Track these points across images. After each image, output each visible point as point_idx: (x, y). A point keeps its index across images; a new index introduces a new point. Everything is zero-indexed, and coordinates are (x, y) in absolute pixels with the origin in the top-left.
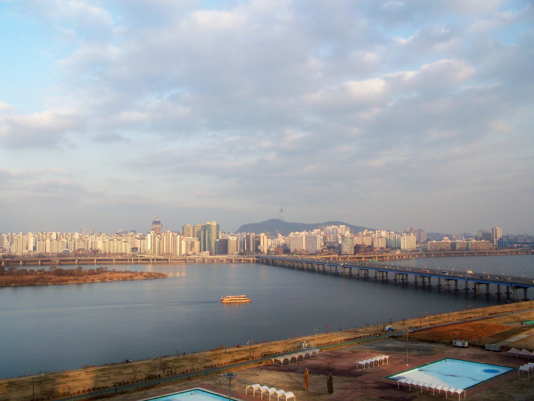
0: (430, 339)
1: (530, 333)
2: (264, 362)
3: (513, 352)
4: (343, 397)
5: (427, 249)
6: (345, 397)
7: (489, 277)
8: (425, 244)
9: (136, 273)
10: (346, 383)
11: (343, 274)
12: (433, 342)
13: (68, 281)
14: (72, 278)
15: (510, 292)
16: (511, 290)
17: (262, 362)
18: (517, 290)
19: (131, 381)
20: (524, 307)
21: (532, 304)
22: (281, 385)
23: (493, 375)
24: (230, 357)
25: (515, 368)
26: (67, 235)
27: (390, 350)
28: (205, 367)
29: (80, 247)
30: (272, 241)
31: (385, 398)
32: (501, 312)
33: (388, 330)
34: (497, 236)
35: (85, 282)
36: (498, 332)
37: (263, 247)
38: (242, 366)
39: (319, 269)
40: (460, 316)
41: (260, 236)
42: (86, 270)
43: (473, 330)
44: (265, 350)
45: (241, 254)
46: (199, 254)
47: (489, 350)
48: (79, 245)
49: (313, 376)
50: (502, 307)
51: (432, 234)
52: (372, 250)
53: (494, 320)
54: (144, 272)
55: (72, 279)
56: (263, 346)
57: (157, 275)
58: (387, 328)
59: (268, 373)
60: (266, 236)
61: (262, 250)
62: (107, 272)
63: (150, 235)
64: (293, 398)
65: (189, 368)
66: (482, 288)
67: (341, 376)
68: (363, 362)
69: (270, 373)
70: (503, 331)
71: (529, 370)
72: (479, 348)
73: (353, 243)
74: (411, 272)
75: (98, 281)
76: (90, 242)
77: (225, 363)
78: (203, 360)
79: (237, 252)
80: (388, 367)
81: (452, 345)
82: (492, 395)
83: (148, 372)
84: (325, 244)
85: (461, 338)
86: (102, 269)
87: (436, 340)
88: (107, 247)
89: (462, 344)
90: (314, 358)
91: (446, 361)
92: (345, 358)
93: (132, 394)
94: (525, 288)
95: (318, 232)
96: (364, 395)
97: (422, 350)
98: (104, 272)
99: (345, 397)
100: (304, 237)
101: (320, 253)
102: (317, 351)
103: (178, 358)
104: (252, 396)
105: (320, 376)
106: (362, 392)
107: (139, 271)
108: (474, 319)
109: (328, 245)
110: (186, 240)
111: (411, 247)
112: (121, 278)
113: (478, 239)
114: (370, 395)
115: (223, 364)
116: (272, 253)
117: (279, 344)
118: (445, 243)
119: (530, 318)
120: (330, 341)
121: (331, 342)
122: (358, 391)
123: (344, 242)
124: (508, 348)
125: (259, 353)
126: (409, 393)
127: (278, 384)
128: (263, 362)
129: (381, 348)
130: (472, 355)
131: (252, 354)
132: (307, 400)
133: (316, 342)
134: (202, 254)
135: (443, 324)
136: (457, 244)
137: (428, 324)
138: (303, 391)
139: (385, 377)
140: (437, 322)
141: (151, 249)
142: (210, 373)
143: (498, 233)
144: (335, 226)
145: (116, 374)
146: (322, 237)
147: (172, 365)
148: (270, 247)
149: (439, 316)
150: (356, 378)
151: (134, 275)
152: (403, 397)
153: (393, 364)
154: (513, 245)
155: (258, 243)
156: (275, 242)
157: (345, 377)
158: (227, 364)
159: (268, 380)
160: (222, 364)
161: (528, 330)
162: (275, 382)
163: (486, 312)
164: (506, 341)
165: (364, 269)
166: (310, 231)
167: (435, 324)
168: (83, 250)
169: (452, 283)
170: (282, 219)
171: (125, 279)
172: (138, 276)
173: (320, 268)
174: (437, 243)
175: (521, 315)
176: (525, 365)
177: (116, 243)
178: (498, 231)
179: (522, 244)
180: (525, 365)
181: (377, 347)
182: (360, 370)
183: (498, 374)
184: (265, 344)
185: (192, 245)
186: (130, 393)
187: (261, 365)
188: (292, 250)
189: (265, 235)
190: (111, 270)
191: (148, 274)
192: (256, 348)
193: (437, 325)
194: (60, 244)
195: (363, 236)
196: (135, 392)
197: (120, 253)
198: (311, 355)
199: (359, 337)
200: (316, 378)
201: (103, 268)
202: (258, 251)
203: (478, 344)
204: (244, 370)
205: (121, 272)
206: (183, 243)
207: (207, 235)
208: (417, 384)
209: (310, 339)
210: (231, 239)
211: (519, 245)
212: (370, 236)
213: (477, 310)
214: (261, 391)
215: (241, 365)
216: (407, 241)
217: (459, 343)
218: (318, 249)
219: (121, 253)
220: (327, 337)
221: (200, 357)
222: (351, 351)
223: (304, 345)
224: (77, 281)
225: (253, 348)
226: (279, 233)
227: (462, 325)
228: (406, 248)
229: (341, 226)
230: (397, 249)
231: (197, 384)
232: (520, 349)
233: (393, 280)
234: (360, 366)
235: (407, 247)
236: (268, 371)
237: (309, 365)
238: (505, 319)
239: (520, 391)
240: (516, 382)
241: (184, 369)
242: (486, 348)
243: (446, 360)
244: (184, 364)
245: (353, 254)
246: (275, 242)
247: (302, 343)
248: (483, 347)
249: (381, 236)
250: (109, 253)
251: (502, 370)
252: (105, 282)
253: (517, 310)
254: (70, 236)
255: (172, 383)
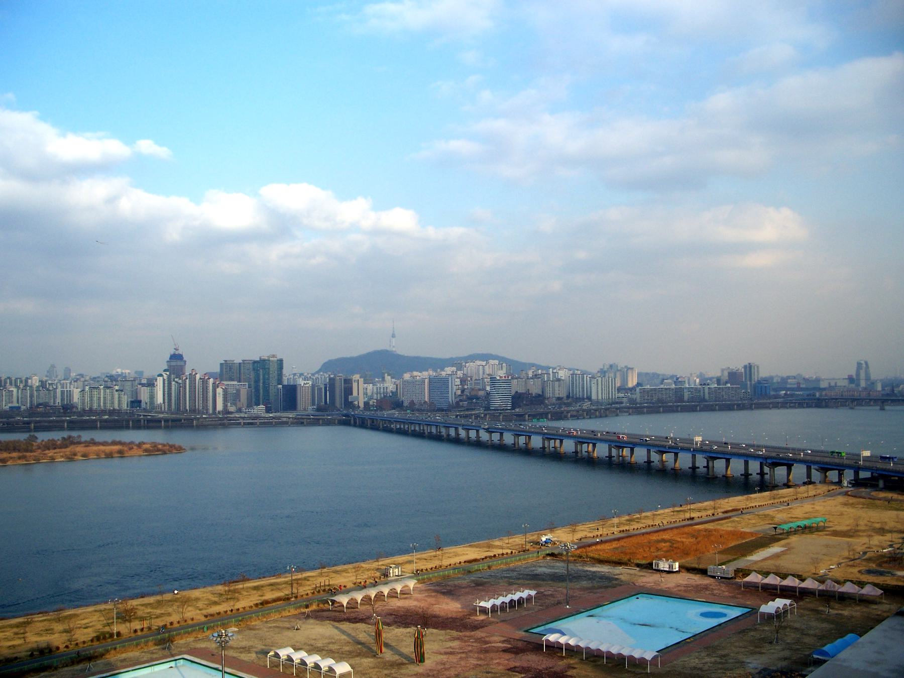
0: (614, 558)
1: (788, 544)
2: (314, 604)
3: (810, 587)
4: (444, 668)
5: (636, 400)
6: (446, 669)
7: (730, 447)
8: (633, 391)
9: (130, 445)
10: (452, 641)
11: (515, 447)
12: (619, 563)
13: (7, 461)
14: (15, 455)
15: (765, 472)
16: (766, 469)
17: (311, 604)
18: (775, 469)
19: (64, 646)
20: (784, 497)
21: (797, 493)
22: (336, 647)
23: (713, 622)
24: (257, 595)
25: (753, 609)
26: (19, 380)
27: (543, 580)
28: (206, 616)
29: (41, 401)
30: (375, 387)
31: (517, 669)
32: (744, 507)
33: (546, 542)
34: (753, 378)
35: (37, 460)
36: (733, 544)
37: (357, 398)
38: (272, 612)
39: (448, 435)
40: (673, 515)
41: (352, 379)
42: (43, 441)
43: (692, 540)
44: (322, 581)
45: (319, 409)
46: (247, 411)
47: (714, 577)
48: (38, 396)
49: (397, 630)
50: (747, 500)
51: (647, 374)
52: (542, 402)
53: (730, 522)
54: (144, 443)
55: (14, 458)
56: (321, 575)
57: (168, 448)
58: (544, 539)
59: (317, 624)
60: (363, 379)
61: (356, 403)
62: (79, 443)
63: (161, 378)
64: (349, 673)
65: (175, 618)
66: (719, 466)
67: (445, 630)
68: (487, 604)
69: (322, 625)
70: (744, 541)
71: (776, 612)
72: (698, 574)
73: (510, 391)
74: (601, 440)
75: (62, 459)
76: (59, 391)
77: (244, 608)
78: (206, 603)
79: (313, 407)
80: (533, 611)
81: (652, 569)
82: (707, 659)
83: (101, 627)
84: (463, 391)
85: (669, 555)
86: (71, 439)
87: (625, 559)
88: (87, 399)
89: (668, 567)
90: (406, 596)
91: (638, 598)
92: (459, 596)
93: (61, 670)
94: (789, 467)
95: (453, 371)
96: (480, 665)
97: (600, 579)
98: (73, 443)
99: (446, 669)
100: (427, 381)
101: (455, 408)
102: (412, 584)
103: (161, 599)
104: (278, 670)
105: (408, 630)
106: (480, 659)
107: (137, 442)
108: (696, 520)
109: (468, 394)
110: (223, 387)
111: (609, 396)
112: (103, 454)
113: (722, 382)
114: (492, 665)
115: (241, 610)
116: (372, 409)
117: (350, 570)
118: (666, 389)
119: (792, 518)
120: (440, 564)
121: (441, 567)
122: (470, 658)
123: (495, 389)
124: (746, 573)
125: (310, 588)
126: (563, 660)
127: (331, 645)
128: (312, 605)
129: (527, 575)
130: (684, 587)
131: (295, 591)
132: (376, 676)
133: (414, 567)
134: (252, 411)
135: (644, 531)
136: (685, 391)
137: (617, 531)
138: (372, 660)
139: (526, 629)
140: (632, 527)
141: (164, 403)
142: (213, 626)
143: (754, 373)
144: (481, 362)
145: (41, 632)
146: (459, 380)
147: (148, 613)
148: (371, 398)
149: (639, 516)
150: (473, 633)
151: (126, 449)
152: (550, 668)
153: (544, 604)
154: (778, 393)
155: (348, 391)
156: (385, 389)
157: (452, 632)
158: (248, 609)
159: (314, 637)
160: (238, 609)
161: (784, 539)
162: (327, 641)
163: (719, 508)
164: (746, 558)
165: (524, 435)
166: (439, 370)
167: (629, 530)
168: (46, 405)
169: (668, 458)
170: (394, 349)
171: (109, 456)
172: (133, 450)
173: (470, 436)
174: (652, 390)
175: (776, 512)
176: (769, 603)
177: (102, 392)
178: (754, 368)
179: (793, 391)
180: (771, 603)
181: (520, 574)
182: (482, 617)
183: (723, 620)
184: (325, 570)
185: (237, 395)
186: (56, 668)
187: (310, 609)
188: (406, 404)
189: (360, 378)
190: (88, 439)
191: (152, 447)
192: (306, 579)
193: (632, 532)
194: (4, 395)
195: (528, 379)
196: (67, 666)
197: (110, 410)
198: (401, 591)
199: (493, 555)
200: (400, 634)
201: (74, 437)
202: (349, 404)
203: (697, 566)
204: (275, 621)
205: (105, 444)
206: (219, 391)
207: (261, 377)
208: (598, 648)
209: (405, 561)
210: (302, 385)
211: (788, 393)
212: (540, 378)
213: (706, 504)
214: (307, 665)
215: (271, 611)
216: (602, 386)
217: (664, 565)
218: (450, 400)
219: (112, 410)
220: (436, 556)
221: (203, 597)
222: (473, 581)
223: (391, 572)
224: (24, 460)
225: (297, 580)
226: (386, 375)
227: (675, 531)
228: (601, 398)
229: (492, 362)
230: (586, 400)
231: (185, 648)
232: (784, 577)
233: (689, 468)
234: (484, 611)
235: (602, 397)
236: (318, 622)
237: (394, 609)
238: (749, 520)
239: (758, 650)
240: (752, 633)
241: (167, 620)
242: (709, 574)
243: (637, 596)
244: (170, 610)
245: (509, 409)
246: (385, 389)
247: (389, 568)
248: (703, 572)
249: (559, 377)
250: (91, 409)
251: (734, 613)
252: (75, 461)
253: (772, 503)
254: (24, 381)
255: (139, 647)
